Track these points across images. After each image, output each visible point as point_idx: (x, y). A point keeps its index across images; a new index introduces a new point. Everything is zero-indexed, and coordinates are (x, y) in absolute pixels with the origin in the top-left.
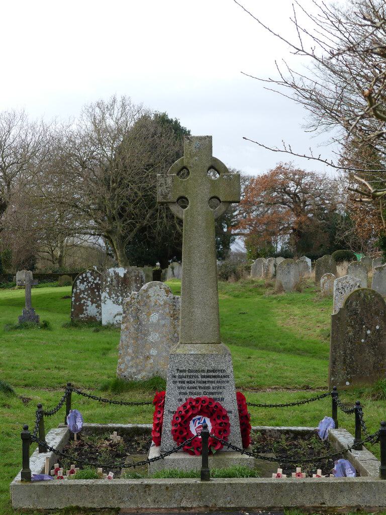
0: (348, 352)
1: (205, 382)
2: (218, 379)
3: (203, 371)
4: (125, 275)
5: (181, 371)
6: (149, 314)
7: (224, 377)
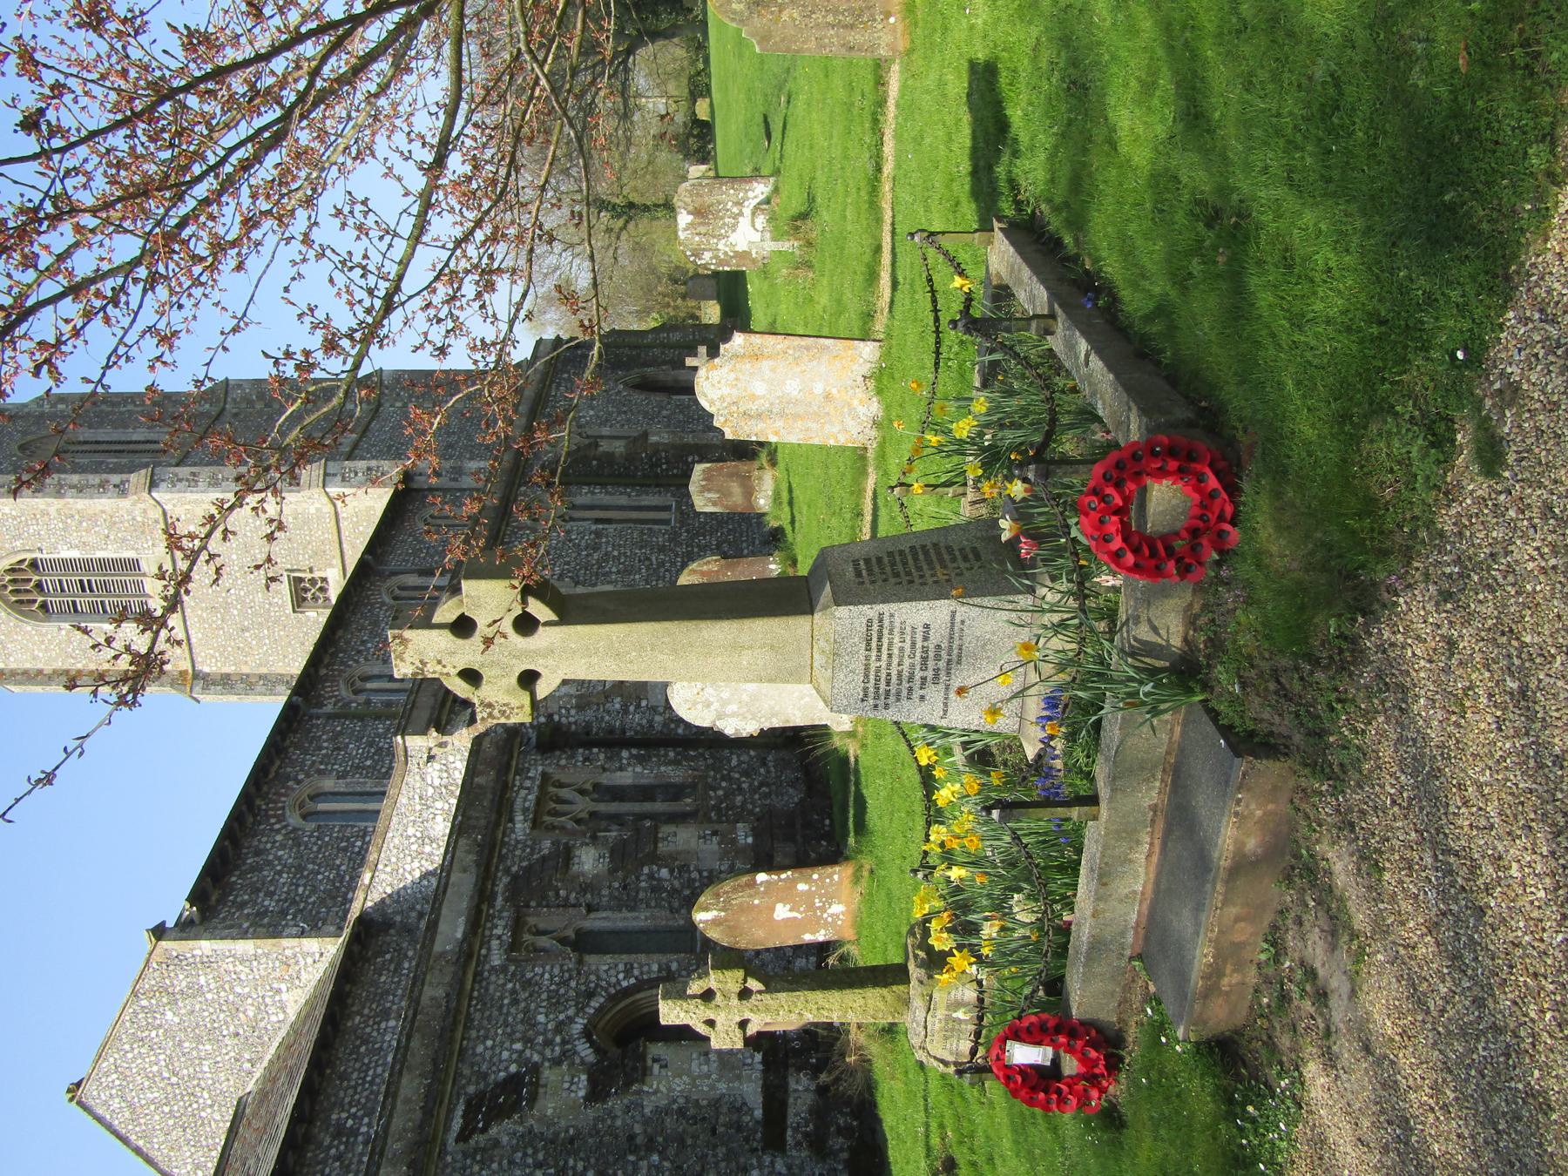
0: (830, 18)
1: (890, 656)
2: (886, 632)
3: (867, 658)
4: (689, 213)
6: (753, 398)
7: (881, 621)
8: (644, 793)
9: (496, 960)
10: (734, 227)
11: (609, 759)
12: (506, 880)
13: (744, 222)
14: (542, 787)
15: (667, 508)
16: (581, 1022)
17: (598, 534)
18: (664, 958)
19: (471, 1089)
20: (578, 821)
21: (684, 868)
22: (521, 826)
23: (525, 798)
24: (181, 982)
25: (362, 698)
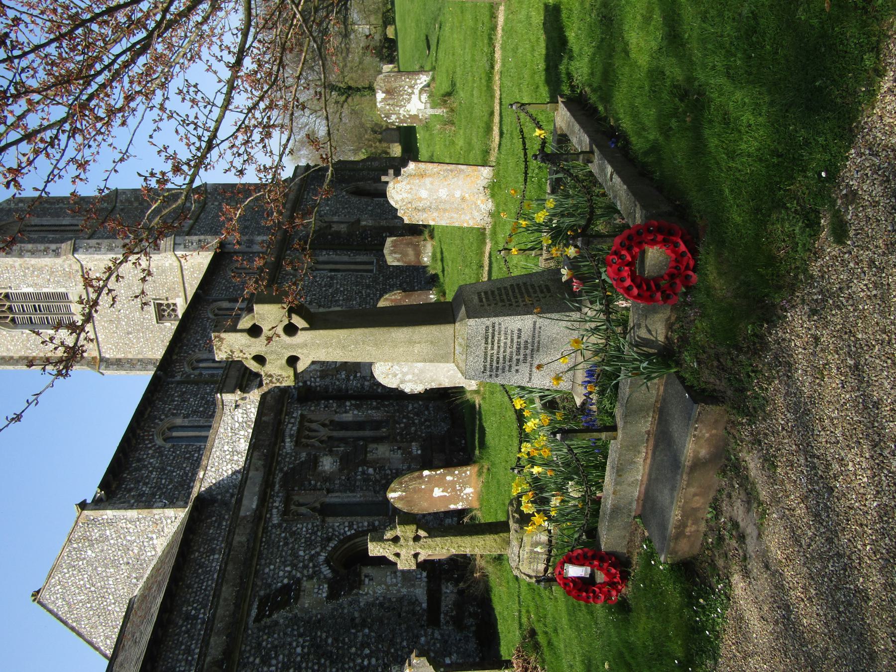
1: (499, 347)
2: (496, 333)
3: (486, 348)
4: (383, 92)
5: (485, 370)
7: (494, 327)
8: (359, 425)
10: (409, 101)
11: (339, 406)
12: (280, 475)
13: (415, 98)
14: (301, 423)
16: (323, 555)
17: (332, 278)
18: (371, 519)
19: (262, 593)
20: (322, 442)
21: (382, 468)
22: (289, 444)
23: (291, 429)
24: (96, 534)
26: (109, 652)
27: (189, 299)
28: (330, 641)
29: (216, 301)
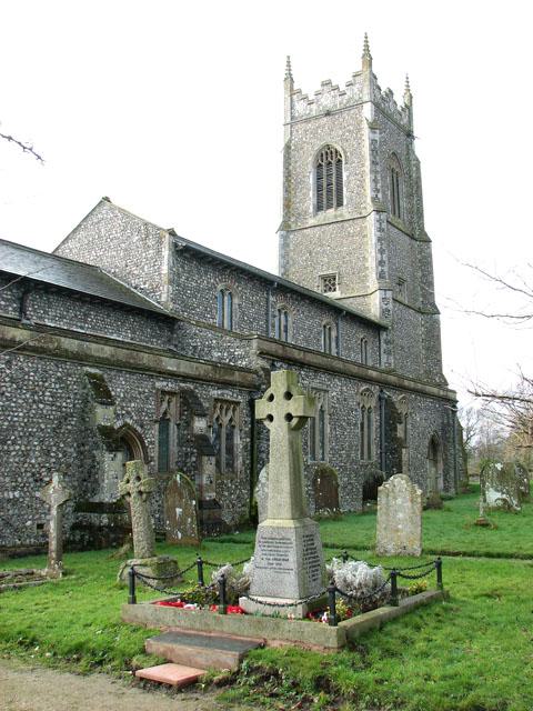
6: (395, 498)
8: (230, 450)
9: (158, 385)
10: (497, 491)
11: (245, 433)
12: (192, 387)
13: (499, 495)
14: (233, 402)
15: (369, 458)
16: (130, 422)
17: (355, 425)
18: (156, 458)
19: (105, 376)
20: (217, 419)
21: (196, 468)
22: (215, 393)
23: (228, 394)
24: (151, 242)
25: (277, 313)
26: (59, 253)
27: (340, 303)
28: (69, 427)
29: (337, 324)
